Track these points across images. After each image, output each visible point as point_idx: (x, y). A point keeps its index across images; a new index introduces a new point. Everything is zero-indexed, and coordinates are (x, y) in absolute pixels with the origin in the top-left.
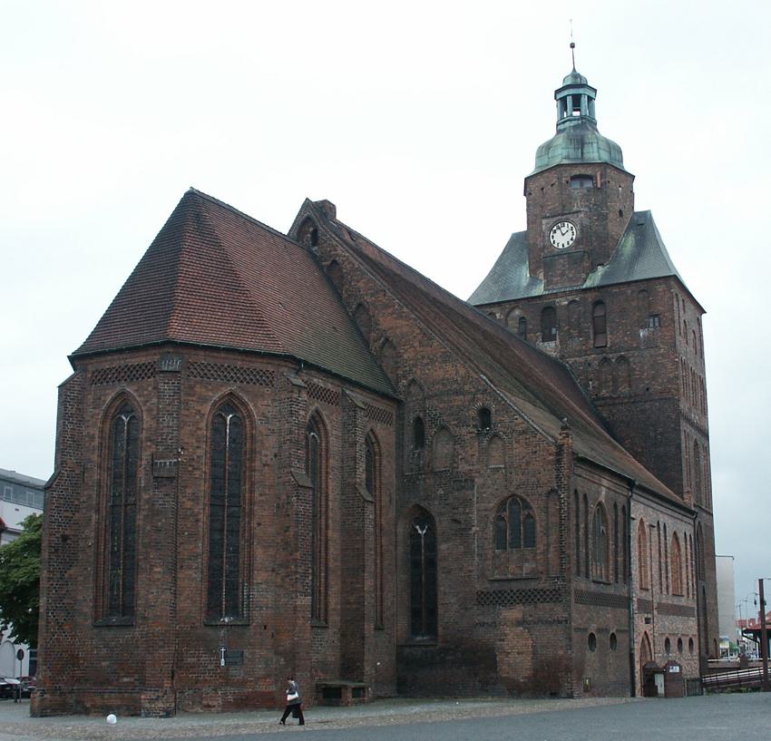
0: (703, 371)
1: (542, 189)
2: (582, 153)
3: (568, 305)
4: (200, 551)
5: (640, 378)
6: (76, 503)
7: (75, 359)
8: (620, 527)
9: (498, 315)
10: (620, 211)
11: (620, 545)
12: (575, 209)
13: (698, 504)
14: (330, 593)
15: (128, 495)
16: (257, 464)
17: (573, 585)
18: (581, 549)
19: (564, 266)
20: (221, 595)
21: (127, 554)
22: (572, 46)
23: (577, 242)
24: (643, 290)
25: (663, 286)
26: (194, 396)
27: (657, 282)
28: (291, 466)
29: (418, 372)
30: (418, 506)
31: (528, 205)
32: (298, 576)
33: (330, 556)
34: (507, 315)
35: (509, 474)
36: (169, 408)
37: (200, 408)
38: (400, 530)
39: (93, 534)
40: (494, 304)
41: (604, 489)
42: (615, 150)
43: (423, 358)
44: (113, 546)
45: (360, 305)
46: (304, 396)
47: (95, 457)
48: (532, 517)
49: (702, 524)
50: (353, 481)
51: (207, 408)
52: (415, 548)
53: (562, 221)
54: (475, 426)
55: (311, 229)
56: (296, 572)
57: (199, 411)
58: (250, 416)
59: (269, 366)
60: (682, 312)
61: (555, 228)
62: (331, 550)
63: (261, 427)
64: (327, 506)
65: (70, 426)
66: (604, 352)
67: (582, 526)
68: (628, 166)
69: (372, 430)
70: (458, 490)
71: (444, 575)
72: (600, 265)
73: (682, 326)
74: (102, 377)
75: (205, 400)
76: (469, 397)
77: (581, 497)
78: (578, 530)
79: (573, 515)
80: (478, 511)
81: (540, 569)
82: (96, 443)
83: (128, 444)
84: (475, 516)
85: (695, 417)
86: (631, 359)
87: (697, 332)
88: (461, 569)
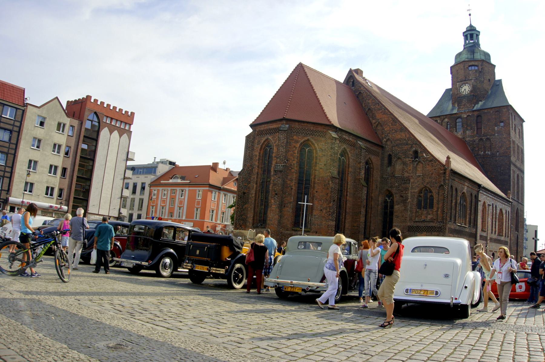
0: (523, 145)
1: (457, 71)
2: (473, 57)
3: (467, 117)
4: (292, 200)
5: (495, 147)
6: (249, 180)
7: (252, 126)
8: (473, 204)
9: (438, 121)
10: (489, 80)
11: (473, 211)
12: (470, 78)
13: (513, 198)
14: (346, 222)
15: (268, 178)
16: (317, 168)
17: (448, 226)
18: (453, 211)
19: (465, 101)
20: (300, 218)
21: (266, 200)
22: (470, 15)
23: (471, 91)
24: (497, 111)
25: (506, 109)
26: (293, 140)
27: (503, 108)
28: (330, 169)
29: (391, 136)
30: (388, 190)
31: (452, 77)
32: (330, 213)
33: (347, 208)
34: (442, 121)
35: (424, 178)
36: (282, 144)
37: (295, 145)
38: (380, 199)
39: (254, 192)
40: (437, 116)
41: (466, 187)
42: (487, 55)
43: (393, 130)
44: (261, 197)
45: (369, 109)
46: (338, 142)
47: (257, 163)
48: (433, 196)
49: (519, 209)
50: (359, 177)
51: (298, 145)
52: (386, 207)
53: (465, 84)
54: (412, 158)
55: (352, 80)
56: (329, 212)
57: (295, 146)
58: (316, 149)
59: (324, 129)
60: (513, 120)
61: (462, 86)
62: (348, 205)
63: (320, 153)
64: (347, 186)
65: (248, 151)
66: (481, 136)
67: (454, 201)
68: (493, 61)
69: (370, 158)
70: (404, 184)
71: (396, 219)
72: (480, 101)
73: (514, 126)
74: (261, 133)
75: (297, 142)
76: (410, 146)
77: (454, 189)
78: (452, 203)
79: (449, 197)
80: (411, 193)
81: (434, 218)
82: (257, 158)
83: (269, 158)
84: (409, 195)
85: (518, 164)
86: (491, 140)
87: (520, 129)
88: (403, 216)
